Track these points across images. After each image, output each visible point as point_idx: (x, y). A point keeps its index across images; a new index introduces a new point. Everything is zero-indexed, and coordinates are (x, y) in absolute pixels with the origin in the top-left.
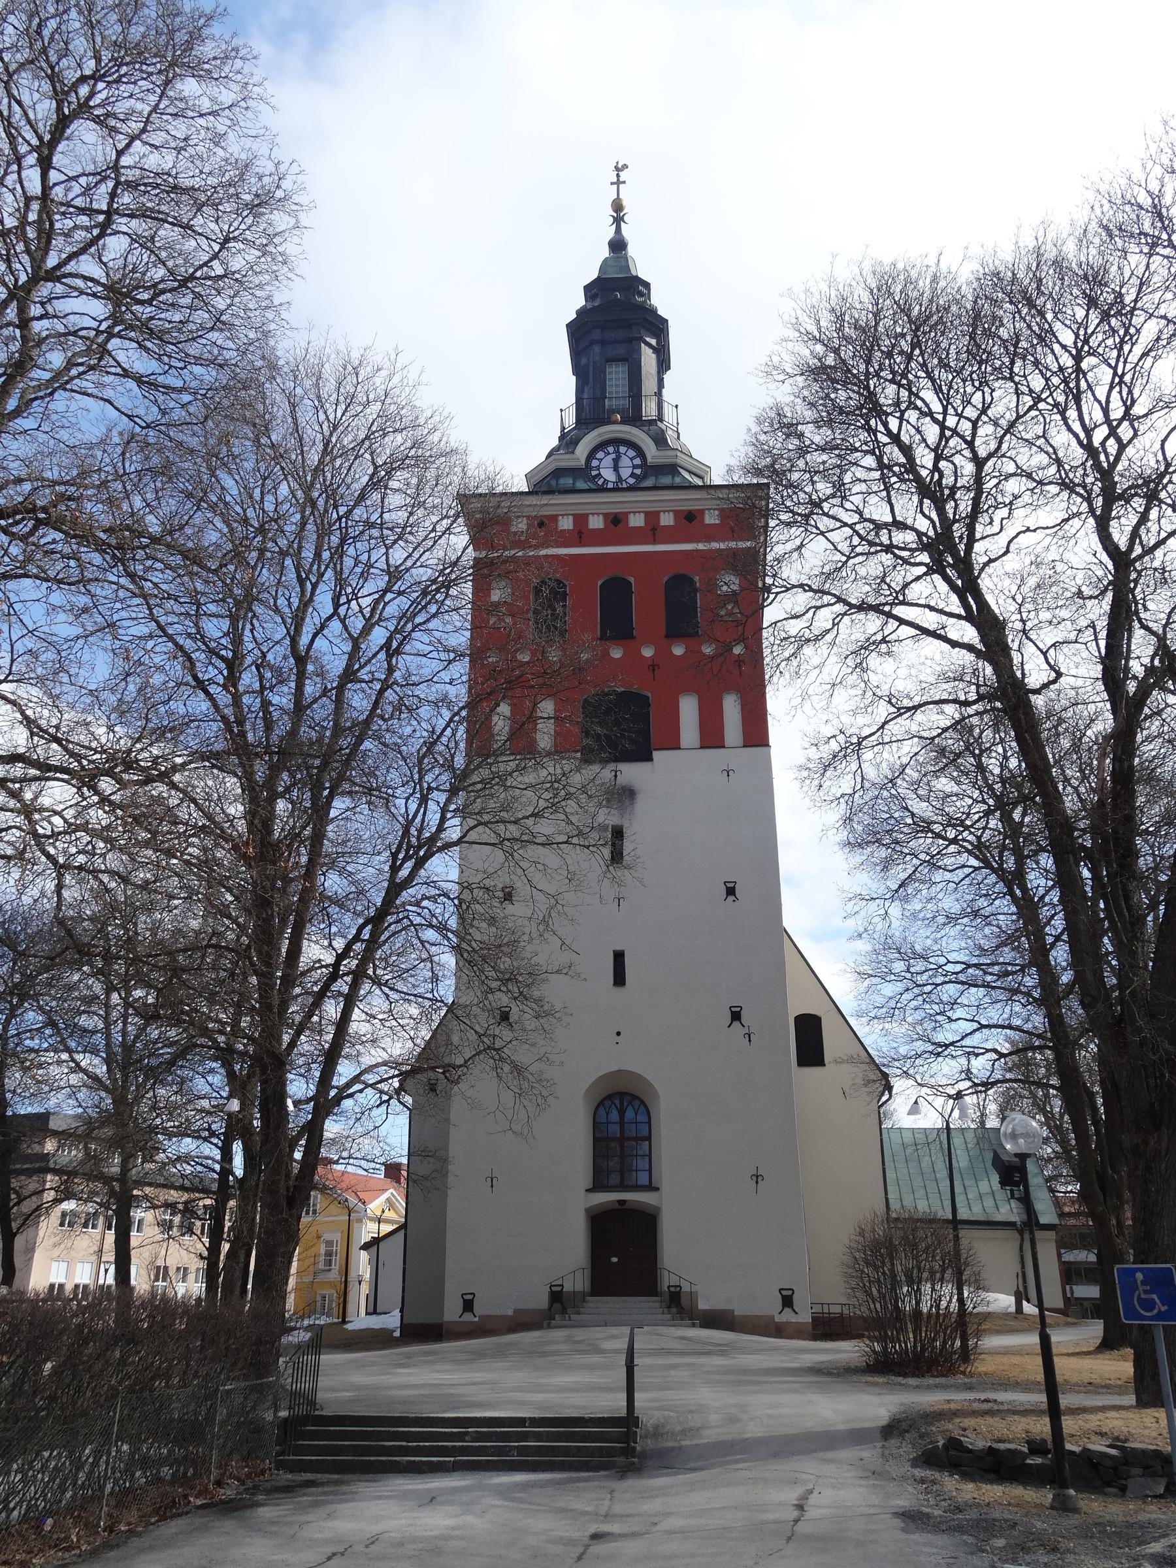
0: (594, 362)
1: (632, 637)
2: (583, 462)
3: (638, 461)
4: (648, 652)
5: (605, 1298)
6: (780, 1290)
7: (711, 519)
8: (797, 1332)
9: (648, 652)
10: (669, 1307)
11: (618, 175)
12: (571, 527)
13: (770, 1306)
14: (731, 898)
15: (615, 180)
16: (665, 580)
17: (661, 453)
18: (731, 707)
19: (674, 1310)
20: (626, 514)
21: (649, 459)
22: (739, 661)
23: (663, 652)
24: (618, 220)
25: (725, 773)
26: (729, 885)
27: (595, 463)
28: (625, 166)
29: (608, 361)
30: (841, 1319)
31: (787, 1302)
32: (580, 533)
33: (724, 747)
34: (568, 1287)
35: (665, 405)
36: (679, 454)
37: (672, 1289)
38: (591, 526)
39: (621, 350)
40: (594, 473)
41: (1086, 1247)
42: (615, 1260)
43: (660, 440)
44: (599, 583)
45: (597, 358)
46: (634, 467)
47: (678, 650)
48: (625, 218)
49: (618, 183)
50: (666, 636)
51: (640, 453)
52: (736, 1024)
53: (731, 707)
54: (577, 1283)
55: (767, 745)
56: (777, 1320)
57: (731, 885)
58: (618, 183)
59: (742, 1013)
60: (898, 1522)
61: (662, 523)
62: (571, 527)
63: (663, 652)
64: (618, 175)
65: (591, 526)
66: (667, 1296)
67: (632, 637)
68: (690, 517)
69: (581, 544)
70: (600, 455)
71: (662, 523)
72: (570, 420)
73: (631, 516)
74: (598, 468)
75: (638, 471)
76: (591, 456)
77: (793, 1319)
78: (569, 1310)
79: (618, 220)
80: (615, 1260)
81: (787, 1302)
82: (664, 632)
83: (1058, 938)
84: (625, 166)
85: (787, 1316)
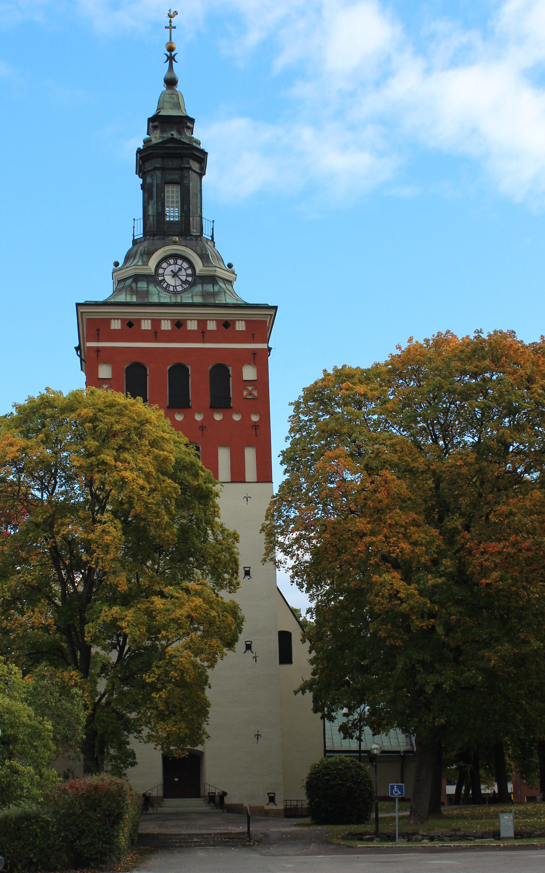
0: (157, 185)
1: (189, 407)
2: (153, 271)
3: (189, 272)
4: (199, 417)
5: (174, 799)
7: (240, 326)
8: (276, 814)
9: (199, 417)
10: (209, 803)
11: (170, 22)
13: (263, 802)
14: (248, 577)
15: (168, 25)
16: (210, 368)
19: (212, 805)
20: (185, 321)
21: (198, 272)
22: (256, 426)
23: (209, 418)
24: (171, 59)
25: (245, 499)
27: (161, 271)
28: (176, 13)
30: (296, 808)
31: (272, 799)
32: (156, 333)
33: (245, 482)
34: (154, 794)
35: (204, 221)
36: (217, 269)
37: (211, 794)
39: (175, 176)
40: (160, 278)
41: (381, 818)
42: (176, 779)
43: (204, 258)
44: (168, 368)
45: (159, 182)
47: (218, 417)
49: (171, 27)
51: (192, 266)
52: (249, 651)
55: (271, 482)
56: (265, 808)
57: (247, 569)
58: (171, 27)
59: (252, 645)
60: (305, 694)
63: (209, 418)
64: (170, 22)
67: (189, 407)
68: (227, 325)
69: (156, 340)
70: (164, 265)
72: (139, 233)
73: (189, 322)
74: (163, 275)
75: (190, 279)
76: (158, 266)
77: (274, 807)
78: (155, 805)
79: (171, 59)
80: (176, 779)
81: (272, 799)
82: (208, 405)
84: (176, 13)
85: (272, 807)
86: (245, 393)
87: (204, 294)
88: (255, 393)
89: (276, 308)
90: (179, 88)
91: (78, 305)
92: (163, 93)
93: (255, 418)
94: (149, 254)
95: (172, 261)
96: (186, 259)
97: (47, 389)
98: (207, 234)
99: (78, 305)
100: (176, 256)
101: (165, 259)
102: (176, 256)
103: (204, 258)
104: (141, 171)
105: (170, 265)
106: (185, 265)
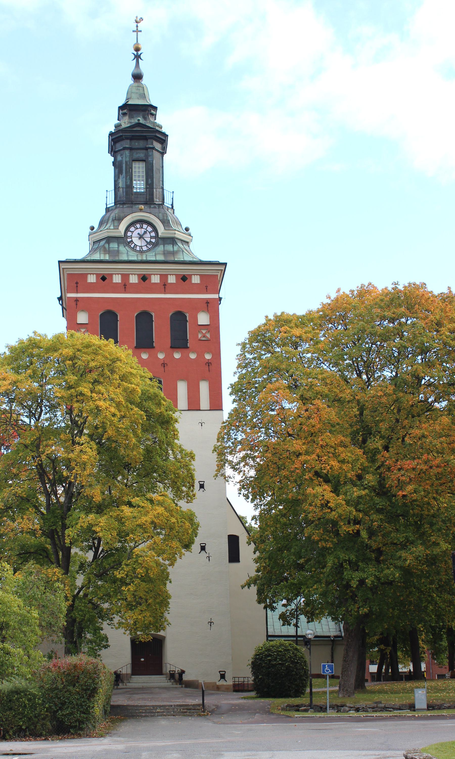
1: (153, 347)
2: (123, 234)
3: (153, 234)
4: (161, 356)
6: (220, 672)
8: (226, 689)
9: (161, 356)
12: (120, 282)
13: (215, 679)
14: (202, 490)
15: (135, 29)
16: (170, 314)
17: (166, 231)
18: (204, 387)
19: (173, 681)
21: (160, 234)
22: (209, 363)
23: (169, 356)
24: (138, 57)
26: (201, 483)
27: (129, 234)
28: (142, 19)
29: (133, 161)
31: (223, 676)
34: (124, 672)
35: (165, 191)
36: (176, 232)
37: (171, 672)
38: (131, 281)
39: (141, 155)
40: (129, 240)
42: (142, 660)
43: (166, 222)
44: (135, 315)
45: (128, 159)
46: (151, 237)
47: (177, 356)
48: (142, 56)
49: (137, 31)
50: (171, 347)
51: (155, 229)
53: (204, 387)
54: (127, 670)
55: (222, 410)
57: (202, 483)
58: (137, 31)
59: (206, 547)
61: (169, 282)
62: (120, 282)
64: (137, 27)
65: (131, 281)
66: (169, 674)
69: (125, 292)
70: (132, 229)
71: (169, 282)
72: (111, 202)
73: (153, 277)
74: (131, 237)
75: (153, 240)
76: (127, 229)
79: (138, 57)
80: (142, 660)
81: (223, 676)
83: (61, 495)
84: (142, 19)
85: (222, 682)
86: (200, 336)
87: (165, 253)
88: (208, 335)
89: (225, 264)
90: (144, 81)
91: (60, 262)
92: (131, 86)
93: (208, 357)
94: (119, 219)
95: (138, 226)
96: (150, 224)
97: (35, 333)
98: (167, 203)
99: (60, 262)
100: (142, 222)
101: (133, 224)
102: (142, 222)
103: (166, 222)
104: (113, 151)
105: (137, 229)
106: (150, 229)
